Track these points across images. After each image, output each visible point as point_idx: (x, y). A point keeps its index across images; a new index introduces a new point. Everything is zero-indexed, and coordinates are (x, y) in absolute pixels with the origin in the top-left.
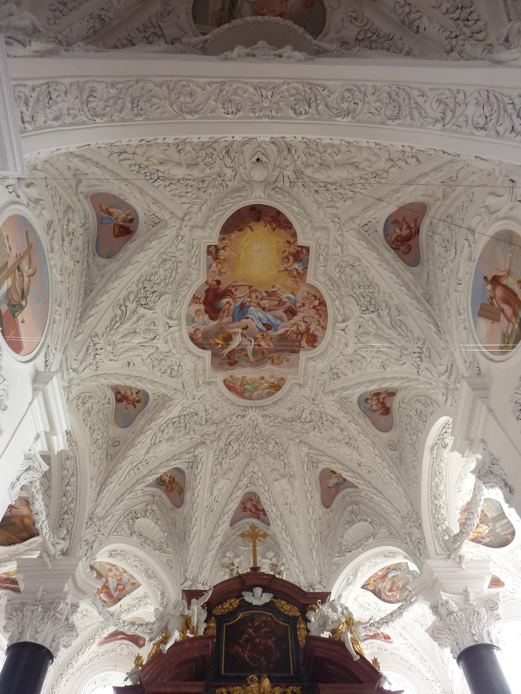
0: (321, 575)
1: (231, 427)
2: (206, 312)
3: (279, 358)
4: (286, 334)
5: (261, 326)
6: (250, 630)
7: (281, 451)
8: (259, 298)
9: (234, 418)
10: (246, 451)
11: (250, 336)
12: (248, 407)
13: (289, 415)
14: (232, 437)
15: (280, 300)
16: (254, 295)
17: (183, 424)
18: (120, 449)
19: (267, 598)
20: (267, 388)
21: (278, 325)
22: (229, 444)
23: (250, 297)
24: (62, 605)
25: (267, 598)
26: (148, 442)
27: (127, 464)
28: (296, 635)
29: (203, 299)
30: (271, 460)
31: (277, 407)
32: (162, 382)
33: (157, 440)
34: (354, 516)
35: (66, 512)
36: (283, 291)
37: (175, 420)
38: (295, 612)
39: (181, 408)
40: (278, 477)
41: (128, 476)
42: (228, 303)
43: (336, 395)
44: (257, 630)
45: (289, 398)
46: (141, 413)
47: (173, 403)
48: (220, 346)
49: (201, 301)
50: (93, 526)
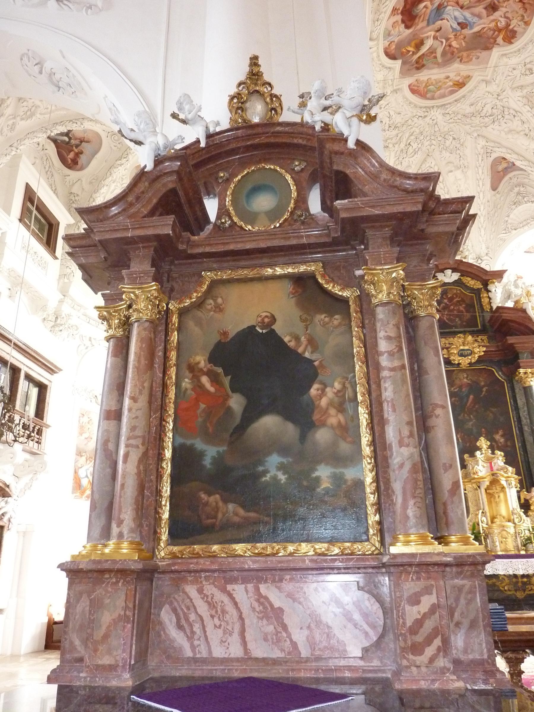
0: (488, 248)
1: (411, 128)
3: (468, 56)
4: (482, 32)
5: (455, 26)
6: (446, 301)
7: (458, 146)
10: (424, 149)
11: (442, 38)
12: (429, 108)
13: (469, 110)
14: (412, 137)
19: (455, 276)
20: (451, 86)
21: (474, 23)
22: (409, 144)
25: (455, 276)
28: (480, 302)
29: (401, 9)
30: (448, 154)
31: (459, 105)
34: (520, 198)
38: (478, 285)
40: (453, 169)
43: (525, 91)
44: (451, 299)
45: (473, 95)
48: (411, 53)
49: (399, 11)
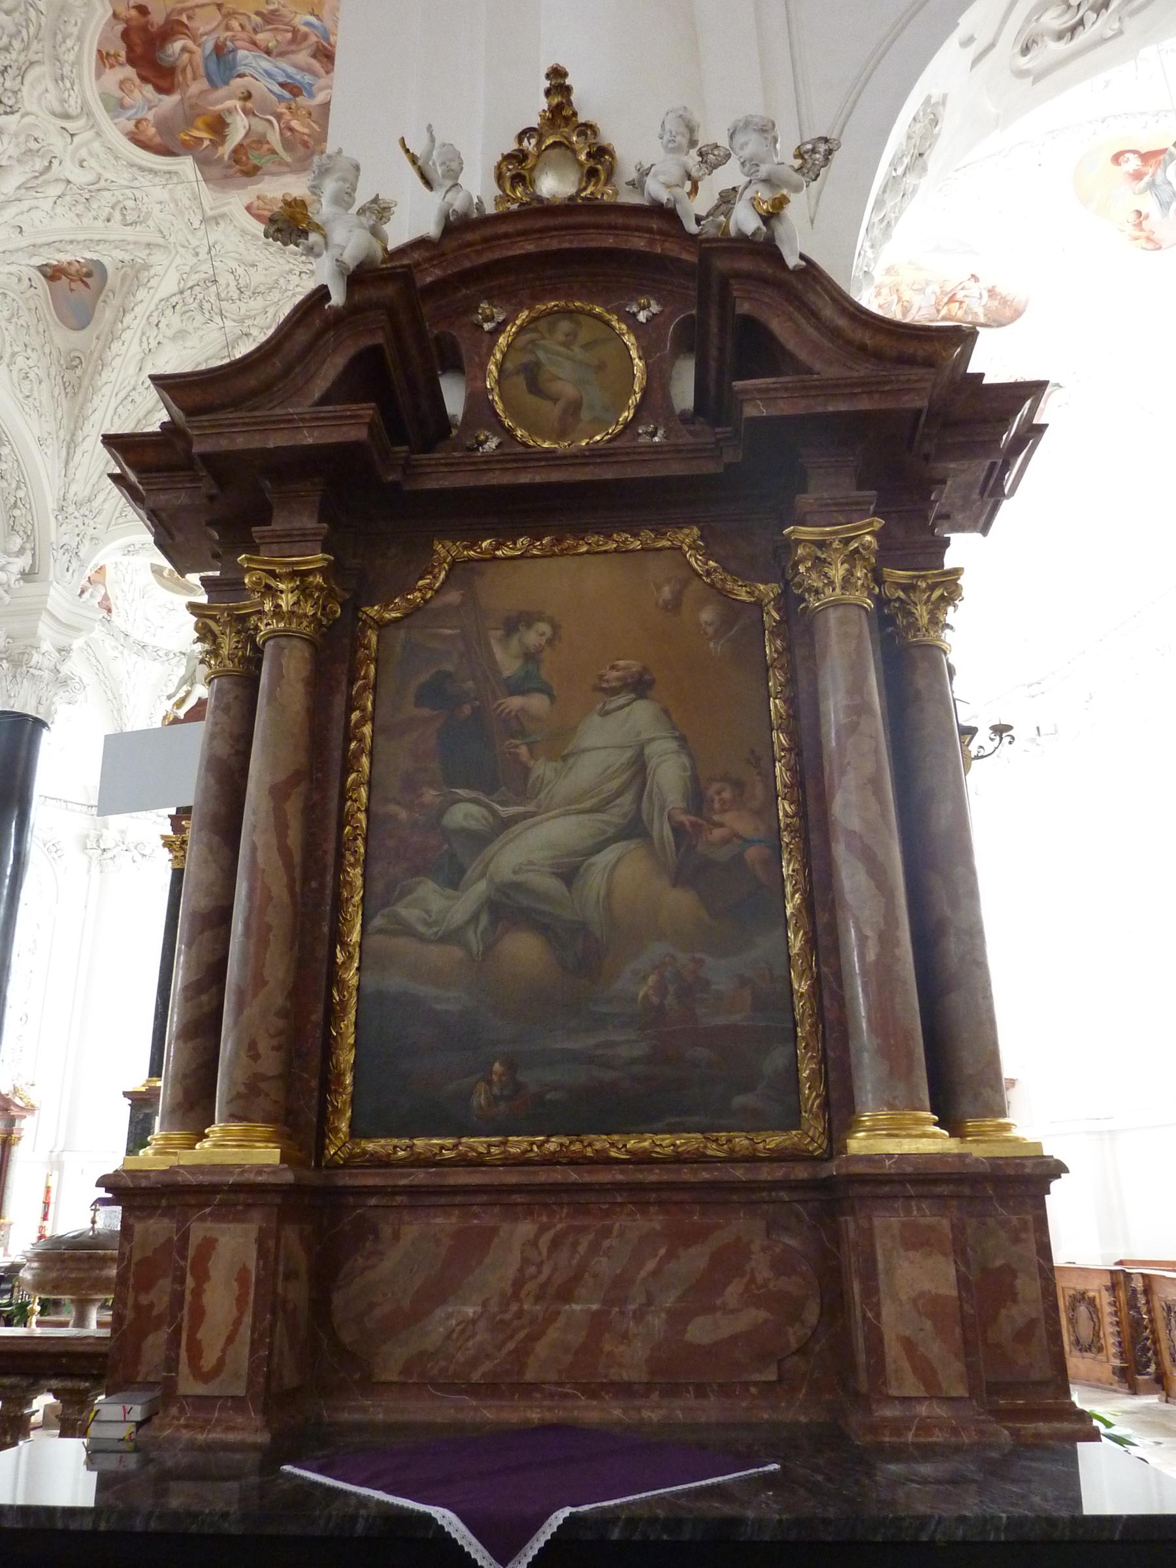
2: (144, 79)
5: (277, 89)
8: (249, 27)
9: (295, 279)
15: (295, 31)
16: (235, 24)
17: (195, 305)
18: (84, 372)
23: (228, 28)
24: (36, 658)
26: (135, 348)
27: (106, 399)
29: (123, 53)
32: (112, 238)
33: (153, 344)
35: (15, 505)
36: (293, 8)
37: (174, 300)
39: (178, 275)
41: (116, 418)
42: (184, 49)
46: (102, 298)
47: (152, 272)
48: (206, 143)
49: (123, 59)
50: (71, 520)
